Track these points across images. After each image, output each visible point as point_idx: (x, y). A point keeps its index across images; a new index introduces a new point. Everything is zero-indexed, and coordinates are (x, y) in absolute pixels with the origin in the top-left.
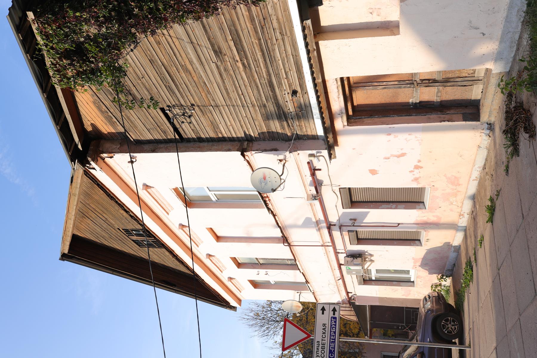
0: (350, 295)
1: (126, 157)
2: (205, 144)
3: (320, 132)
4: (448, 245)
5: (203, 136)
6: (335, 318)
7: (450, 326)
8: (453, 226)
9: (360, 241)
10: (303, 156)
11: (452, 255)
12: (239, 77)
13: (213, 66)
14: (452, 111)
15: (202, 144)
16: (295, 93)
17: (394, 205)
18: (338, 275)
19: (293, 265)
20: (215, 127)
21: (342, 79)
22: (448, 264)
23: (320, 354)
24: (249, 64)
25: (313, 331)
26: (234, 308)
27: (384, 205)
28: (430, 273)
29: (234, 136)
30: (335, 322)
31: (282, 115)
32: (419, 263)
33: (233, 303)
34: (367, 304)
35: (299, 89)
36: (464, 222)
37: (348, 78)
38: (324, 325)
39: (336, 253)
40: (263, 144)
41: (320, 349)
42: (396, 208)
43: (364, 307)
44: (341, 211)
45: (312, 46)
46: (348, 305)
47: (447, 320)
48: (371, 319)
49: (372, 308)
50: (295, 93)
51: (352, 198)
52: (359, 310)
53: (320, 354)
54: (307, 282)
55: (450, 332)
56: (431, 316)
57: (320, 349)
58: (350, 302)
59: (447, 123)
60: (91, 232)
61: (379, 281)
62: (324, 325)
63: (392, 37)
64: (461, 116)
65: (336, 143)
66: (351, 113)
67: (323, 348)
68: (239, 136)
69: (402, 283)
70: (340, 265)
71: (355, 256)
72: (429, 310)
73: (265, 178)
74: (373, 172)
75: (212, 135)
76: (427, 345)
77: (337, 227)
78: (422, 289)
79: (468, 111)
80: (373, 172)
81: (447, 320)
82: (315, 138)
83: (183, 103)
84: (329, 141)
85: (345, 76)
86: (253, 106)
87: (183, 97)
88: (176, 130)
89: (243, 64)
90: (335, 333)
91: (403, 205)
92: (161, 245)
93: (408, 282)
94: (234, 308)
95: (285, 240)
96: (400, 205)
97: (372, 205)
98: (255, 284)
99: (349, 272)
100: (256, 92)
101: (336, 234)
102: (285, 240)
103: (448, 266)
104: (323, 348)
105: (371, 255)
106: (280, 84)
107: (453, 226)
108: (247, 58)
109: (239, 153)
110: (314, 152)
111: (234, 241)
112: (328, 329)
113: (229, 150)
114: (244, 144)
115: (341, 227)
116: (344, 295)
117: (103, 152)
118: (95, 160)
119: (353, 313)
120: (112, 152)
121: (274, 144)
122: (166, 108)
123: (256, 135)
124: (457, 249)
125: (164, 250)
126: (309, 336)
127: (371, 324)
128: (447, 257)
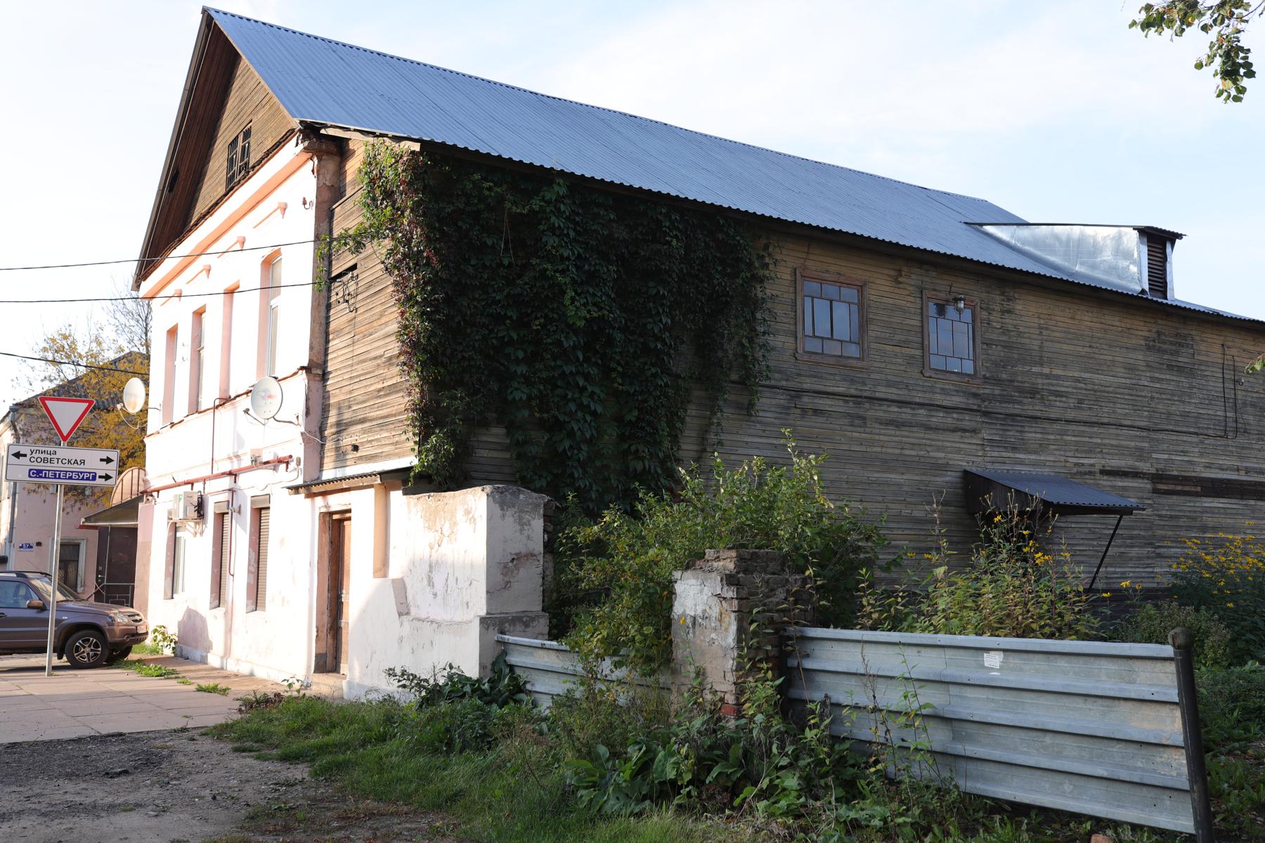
0: (155, 494)
1: (312, 196)
2: (323, 314)
3: (328, 474)
4: (208, 648)
5: (332, 312)
6: (94, 478)
7: (88, 649)
8: (227, 653)
9: (221, 516)
10: (298, 450)
11: (197, 654)
12: (372, 381)
13: (380, 352)
14: (330, 641)
15: (323, 308)
16: (356, 448)
17: (253, 569)
18: (179, 480)
19: (195, 409)
20: (339, 332)
21: (349, 511)
22: (187, 649)
23: (36, 456)
24: (380, 397)
25: (71, 445)
26: (137, 286)
27: (254, 555)
28: (180, 623)
29: (330, 357)
30: (88, 479)
31: (342, 427)
32: (192, 607)
33: (147, 286)
34: (141, 523)
35: (359, 454)
36: (232, 667)
37: (349, 519)
38: (83, 462)
39: (204, 480)
40: (317, 397)
41: (43, 456)
42: (249, 572)
43: (135, 517)
44: (249, 493)
45: (366, 481)
46: (141, 489)
47: (96, 646)
48: (113, 528)
49: (134, 531)
50: (356, 448)
51: (260, 512)
52: (130, 508)
53: (36, 456)
54: (173, 425)
55: (77, 649)
56: (102, 623)
57: (43, 456)
58: (146, 494)
59: (314, 634)
60: (248, 78)
61: (174, 543)
62: (83, 462)
63: (371, 571)
64: (323, 651)
65: (311, 495)
66: (336, 517)
67: (45, 460)
68: (329, 364)
69: (170, 580)
70: (192, 483)
71: (200, 507)
72: (113, 619)
73: (270, 397)
74: (282, 542)
75: (332, 326)
76: (52, 615)
77: (233, 485)
78: (158, 611)
79: (329, 660)
80: (282, 542)
81: (96, 646)
82: (321, 470)
83: (360, 297)
84: (311, 488)
85: (352, 515)
86: (351, 392)
87: (368, 297)
88: (340, 275)
89: (380, 390)
90: (70, 478)
91: (253, 582)
92: (232, 186)
93: (172, 590)
94: (137, 286)
95: (225, 400)
96: (253, 577)
97: (255, 538)
98: (173, 333)
99: (178, 498)
100: (361, 398)
101: (226, 482)
102: (225, 400)
103: (187, 650)
104: (45, 460)
105: (202, 533)
106: (364, 431)
107: (227, 653)
108: (385, 395)
109: (306, 364)
110: (302, 466)
111: (225, 317)
112: (76, 468)
113: (311, 348)
114: (317, 370)
115: (232, 491)
116: (154, 484)
117: (320, 160)
118: (306, 149)
119: (127, 498)
120: (318, 172)
121: (316, 411)
122: (355, 273)
123: (329, 388)
124: (204, 661)
125: (223, 192)
126: (65, 439)
127: (106, 528)
128: (196, 648)
